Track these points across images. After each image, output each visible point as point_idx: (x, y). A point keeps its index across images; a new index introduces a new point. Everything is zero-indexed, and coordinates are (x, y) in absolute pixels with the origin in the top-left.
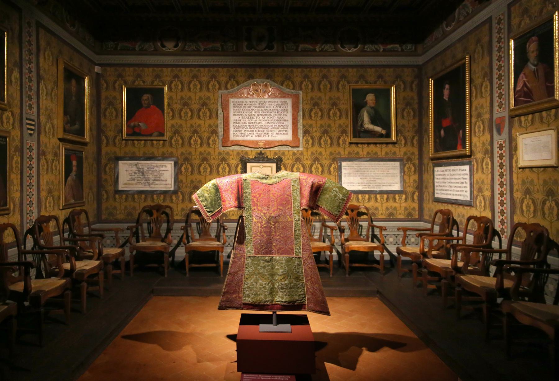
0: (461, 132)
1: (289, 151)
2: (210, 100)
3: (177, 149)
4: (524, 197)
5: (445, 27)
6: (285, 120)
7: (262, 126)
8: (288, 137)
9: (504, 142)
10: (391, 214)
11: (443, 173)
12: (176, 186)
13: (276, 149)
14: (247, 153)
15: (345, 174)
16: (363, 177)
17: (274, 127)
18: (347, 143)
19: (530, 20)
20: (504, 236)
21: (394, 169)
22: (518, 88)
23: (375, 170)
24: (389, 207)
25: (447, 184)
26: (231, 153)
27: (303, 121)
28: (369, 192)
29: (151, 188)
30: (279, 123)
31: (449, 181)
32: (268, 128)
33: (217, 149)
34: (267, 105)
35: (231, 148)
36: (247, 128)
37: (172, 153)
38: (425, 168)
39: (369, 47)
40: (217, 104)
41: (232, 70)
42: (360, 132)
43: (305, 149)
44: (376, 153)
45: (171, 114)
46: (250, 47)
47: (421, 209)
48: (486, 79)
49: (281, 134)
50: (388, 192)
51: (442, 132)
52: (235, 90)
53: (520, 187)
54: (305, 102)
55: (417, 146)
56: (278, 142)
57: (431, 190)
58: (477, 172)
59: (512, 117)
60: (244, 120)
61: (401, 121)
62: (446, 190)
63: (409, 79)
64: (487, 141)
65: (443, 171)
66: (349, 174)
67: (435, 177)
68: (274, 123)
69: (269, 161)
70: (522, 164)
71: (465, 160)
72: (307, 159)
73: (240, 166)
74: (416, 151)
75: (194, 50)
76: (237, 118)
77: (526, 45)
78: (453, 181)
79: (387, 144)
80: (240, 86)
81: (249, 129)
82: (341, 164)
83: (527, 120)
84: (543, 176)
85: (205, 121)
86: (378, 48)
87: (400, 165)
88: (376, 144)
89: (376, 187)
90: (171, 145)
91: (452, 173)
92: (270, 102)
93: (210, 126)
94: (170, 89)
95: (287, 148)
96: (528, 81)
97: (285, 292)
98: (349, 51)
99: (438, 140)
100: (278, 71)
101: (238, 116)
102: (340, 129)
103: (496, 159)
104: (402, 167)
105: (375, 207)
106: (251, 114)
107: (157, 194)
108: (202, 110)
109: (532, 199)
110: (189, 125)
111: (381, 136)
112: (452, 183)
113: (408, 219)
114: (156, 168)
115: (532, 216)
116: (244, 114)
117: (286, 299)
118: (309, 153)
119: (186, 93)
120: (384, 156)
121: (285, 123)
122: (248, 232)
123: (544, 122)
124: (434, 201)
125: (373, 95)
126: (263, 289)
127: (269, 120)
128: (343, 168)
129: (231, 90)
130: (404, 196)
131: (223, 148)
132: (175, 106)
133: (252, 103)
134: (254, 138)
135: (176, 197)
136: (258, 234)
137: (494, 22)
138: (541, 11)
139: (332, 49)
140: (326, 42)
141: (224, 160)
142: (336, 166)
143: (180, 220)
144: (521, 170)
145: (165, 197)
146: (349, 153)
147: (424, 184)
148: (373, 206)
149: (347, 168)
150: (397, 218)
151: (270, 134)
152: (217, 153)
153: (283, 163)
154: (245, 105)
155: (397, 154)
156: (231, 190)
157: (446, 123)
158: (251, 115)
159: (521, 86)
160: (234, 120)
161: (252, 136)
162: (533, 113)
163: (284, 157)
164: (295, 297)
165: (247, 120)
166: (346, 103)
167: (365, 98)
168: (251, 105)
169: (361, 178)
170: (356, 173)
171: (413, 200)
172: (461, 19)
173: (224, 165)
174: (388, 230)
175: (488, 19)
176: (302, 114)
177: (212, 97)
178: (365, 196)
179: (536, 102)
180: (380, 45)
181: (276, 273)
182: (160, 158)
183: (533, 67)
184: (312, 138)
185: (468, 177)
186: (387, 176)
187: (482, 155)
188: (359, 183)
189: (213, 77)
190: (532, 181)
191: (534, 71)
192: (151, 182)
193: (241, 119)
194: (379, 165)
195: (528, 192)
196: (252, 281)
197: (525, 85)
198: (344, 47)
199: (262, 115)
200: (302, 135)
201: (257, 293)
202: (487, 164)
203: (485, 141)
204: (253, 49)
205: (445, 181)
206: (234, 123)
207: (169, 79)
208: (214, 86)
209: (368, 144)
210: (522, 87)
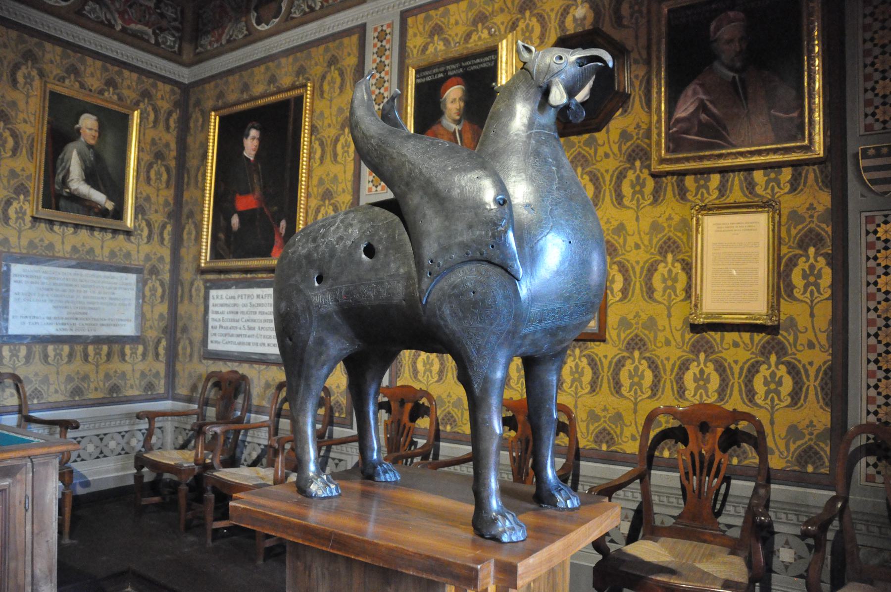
0: (283, 224)
10: (115, 388)
11: (232, 301)
16: (60, 304)
18: (28, 219)
19: (445, 45)
21: (125, 289)
23: (88, 289)
24: (111, 373)
25: (240, 324)
28: (71, 340)
31: (246, 317)
38: (183, 291)
42: (59, 196)
44: (91, 251)
47: (171, 375)
50: (111, 340)
51: (235, 221)
55: (169, 245)
57: (197, 335)
61: (147, 190)
62: (238, 336)
63: (165, 105)
65: (233, 298)
66: (28, 296)
67: (211, 308)
74: (166, 253)
78: (257, 317)
79: (115, 232)
82: (9, 270)
87: (138, 282)
88: (92, 228)
89: (86, 327)
91: (255, 301)
99: (222, 236)
102: (12, 182)
104: (140, 285)
105: (82, 373)
111: (104, 213)
112: (254, 321)
113: (148, 397)
124: (205, 358)
125: (94, 118)
130: (141, 348)
137: (371, 35)
146: (31, 244)
147: (180, 324)
148: (78, 373)
149: (24, 279)
150: (125, 396)
155: (133, 258)
157: (246, 202)
167: (77, 122)
169: (55, 307)
170: (46, 292)
171: (157, 355)
172: (295, 16)
174: (81, 427)
175: (357, 26)
178: (62, 350)
186: (112, 304)
188: (49, 318)
194: (95, 279)
205: (239, 316)
209: (77, 226)
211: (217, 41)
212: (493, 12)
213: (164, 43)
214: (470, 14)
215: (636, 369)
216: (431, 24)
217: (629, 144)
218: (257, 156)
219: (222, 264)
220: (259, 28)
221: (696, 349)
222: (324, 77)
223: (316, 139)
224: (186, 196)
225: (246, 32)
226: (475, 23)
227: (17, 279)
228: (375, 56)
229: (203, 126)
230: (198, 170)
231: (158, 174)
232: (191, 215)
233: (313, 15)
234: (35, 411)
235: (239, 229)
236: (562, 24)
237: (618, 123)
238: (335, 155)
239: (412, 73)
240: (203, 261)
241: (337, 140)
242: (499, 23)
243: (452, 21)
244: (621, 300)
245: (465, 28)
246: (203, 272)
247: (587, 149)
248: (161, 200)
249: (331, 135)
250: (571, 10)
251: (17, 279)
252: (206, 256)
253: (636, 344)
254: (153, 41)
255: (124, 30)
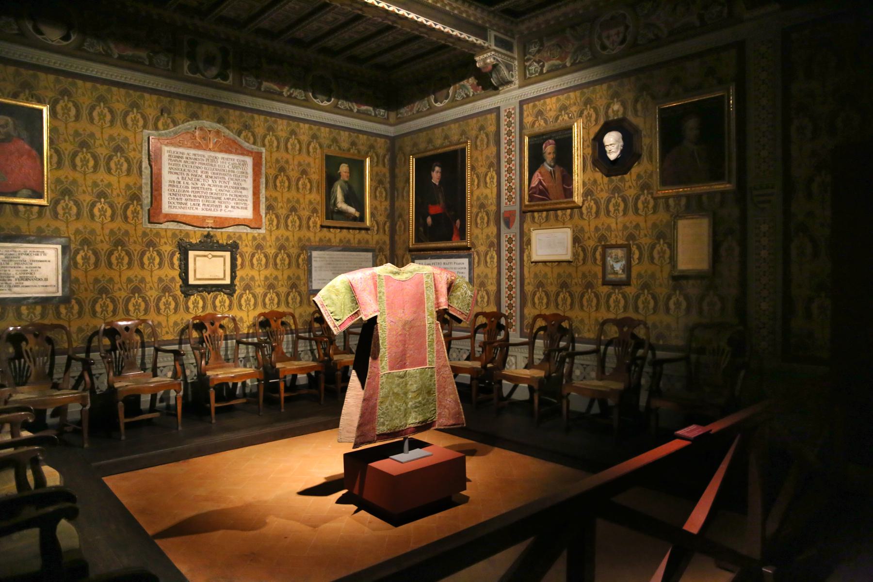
0: (458, 222)
1: (247, 234)
2: (129, 144)
3: (67, 223)
4: (536, 289)
5: (433, 101)
6: (244, 189)
7: (212, 194)
8: (247, 213)
9: (514, 236)
12: (67, 290)
13: (230, 230)
14: (187, 234)
15: (316, 267)
17: (228, 197)
18: (318, 226)
20: (512, 330)
22: (534, 185)
26: (163, 233)
27: (266, 191)
29: (15, 293)
30: (235, 192)
32: (220, 198)
33: (139, 227)
34: (219, 163)
35: (163, 226)
36: (190, 196)
37: (57, 229)
39: (343, 104)
40: (141, 152)
41: (166, 100)
42: (333, 212)
43: (268, 233)
45: (55, 159)
46: (194, 69)
48: (492, 169)
49: (238, 207)
51: (429, 220)
52: (170, 132)
53: (532, 280)
54: (268, 165)
56: (234, 219)
58: (478, 265)
59: (523, 213)
60: (185, 182)
63: (381, 152)
64: (492, 233)
68: (229, 191)
69: (221, 248)
70: (535, 258)
71: (466, 253)
72: (270, 246)
73: (177, 255)
75: (100, 53)
76: (174, 177)
77: (542, 145)
79: (360, 229)
80: (178, 127)
81: (192, 198)
82: (311, 255)
83: (541, 216)
84: (557, 270)
85: (119, 178)
86: (352, 108)
87: (373, 257)
88: (348, 228)
90: (56, 215)
92: (223, 158)
93: (128, 187)
94: (53, 113)
95: (246, 229)
96: (543, 180)
97: (418, 410)
98: (321, 104)
99: (421, 229)
100: (234, 114)
101: (176, 176)
103: (504, 253)
106: (196, 173)
107: (27, 305)
108: (115, 159)
109: (545, 291)
110: (89, 183)
111: (355, 219)
114: (23, 257)
115: (545, 307)
116: (185, 173)
117: (420, 418)
118: (274, 238)
119: (84, 126)
120: (356, 245)
121: (244, 192)
122: (382, 343)
123: (558, 220)
125: (346, 165)
126: (398, 412)
127: (221, 186)
128: (313, 259)
129: (163, 132)
131: (150, 226)
132: (63, 146)
133: (197, 157)
134: (200, 212)
135: (66, 308)
136: (393, 344)
137: (503, 114)
138: (557, 118)
139: (302, 97)
140: (296, 86)
141: (151, 244)
142: (306, 257)
143: (173, 340)
144: (534, 264)
145: (44, 308)
149: (318, 259)
151: (223, 208)
152: (139, 233)
153: (239, 251)
154: (187, 158)
156: (368, 289)
158: (196, 176)
159: (537, 183)
160: (170, 181)
161: (197, 209)
162: (547, 211)
163: (240, 243)
164: (427, 414)
165: (190, 182)
166: (317, 172)
167: (338, 169)
168: (196, 159)
170: (328, 266)
173: (151, 253)
176: (264, 182)
177: (131, 139)
179: (552, 201)
180: (354, 104)
181: (409, 390)
182: (33, 238)
183: (550, 168)
184: (277, 217)
185: (467, 271)
187: (485, 248)
189: (134, 105)
190: (546, 274)
191: (551, 172)
192: (13, 282)
193: (180, 180)
195: (540, 285)
196: (387, 404)
197: (540, 183)
198: (316, 98)
199: (211, 177)
200: (264, 212)
201: (392, 418)
202: (492, 257)
203: (490, 234)
204: (198, 74)
206: (170, 185)
207: (50, 94)
208: (135, 121)
209: (341, 228)
210: (538, 184)
211: (411, 111)
212: (570, 104)
213: (379, 114)
214: (558, 105)
215: (646, 299)
216: (536, 109)
217: (641, 181)
218: (440, 182)
219: (422, 246)
220: (436, 105)
221: (674, 289)
222: (477, 137)
223: (474, 174)
224: (397, 204)
225: (428, 107)
226: (561, 110)
227: (315, 259)
228: (506, 126)
229: (405, 162)
230: (404, 189)
231: (381, 193)
232: (400, 216)
233: (467, 100)
234: (301, 333)
235: (432, 225)
236: (607, 113)
237: (635, 170)
238: (486, 183)
239: (526, 139)
240: (411, 244)
241: (486, 175)
242: (573, 111)
243: (548, 109)
244: (638, 264)
245: (555, 113)
246: (411, 250)
247: (621, 184)
248: (383, 207)
249: (483, 171)
250: (612, 106)
251: (315, 259)
252: (412, 241)
253: (645, 286)
254: (373, 114)
255: (358, 111)
